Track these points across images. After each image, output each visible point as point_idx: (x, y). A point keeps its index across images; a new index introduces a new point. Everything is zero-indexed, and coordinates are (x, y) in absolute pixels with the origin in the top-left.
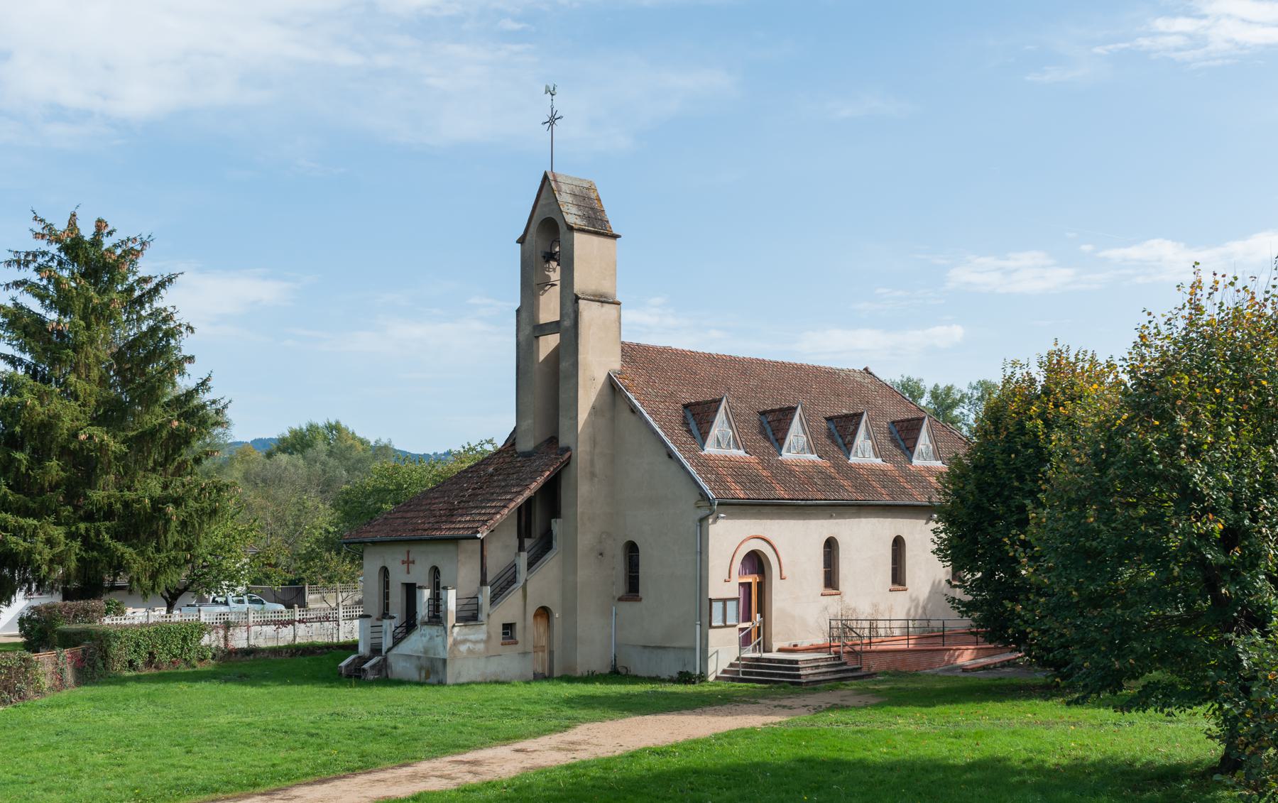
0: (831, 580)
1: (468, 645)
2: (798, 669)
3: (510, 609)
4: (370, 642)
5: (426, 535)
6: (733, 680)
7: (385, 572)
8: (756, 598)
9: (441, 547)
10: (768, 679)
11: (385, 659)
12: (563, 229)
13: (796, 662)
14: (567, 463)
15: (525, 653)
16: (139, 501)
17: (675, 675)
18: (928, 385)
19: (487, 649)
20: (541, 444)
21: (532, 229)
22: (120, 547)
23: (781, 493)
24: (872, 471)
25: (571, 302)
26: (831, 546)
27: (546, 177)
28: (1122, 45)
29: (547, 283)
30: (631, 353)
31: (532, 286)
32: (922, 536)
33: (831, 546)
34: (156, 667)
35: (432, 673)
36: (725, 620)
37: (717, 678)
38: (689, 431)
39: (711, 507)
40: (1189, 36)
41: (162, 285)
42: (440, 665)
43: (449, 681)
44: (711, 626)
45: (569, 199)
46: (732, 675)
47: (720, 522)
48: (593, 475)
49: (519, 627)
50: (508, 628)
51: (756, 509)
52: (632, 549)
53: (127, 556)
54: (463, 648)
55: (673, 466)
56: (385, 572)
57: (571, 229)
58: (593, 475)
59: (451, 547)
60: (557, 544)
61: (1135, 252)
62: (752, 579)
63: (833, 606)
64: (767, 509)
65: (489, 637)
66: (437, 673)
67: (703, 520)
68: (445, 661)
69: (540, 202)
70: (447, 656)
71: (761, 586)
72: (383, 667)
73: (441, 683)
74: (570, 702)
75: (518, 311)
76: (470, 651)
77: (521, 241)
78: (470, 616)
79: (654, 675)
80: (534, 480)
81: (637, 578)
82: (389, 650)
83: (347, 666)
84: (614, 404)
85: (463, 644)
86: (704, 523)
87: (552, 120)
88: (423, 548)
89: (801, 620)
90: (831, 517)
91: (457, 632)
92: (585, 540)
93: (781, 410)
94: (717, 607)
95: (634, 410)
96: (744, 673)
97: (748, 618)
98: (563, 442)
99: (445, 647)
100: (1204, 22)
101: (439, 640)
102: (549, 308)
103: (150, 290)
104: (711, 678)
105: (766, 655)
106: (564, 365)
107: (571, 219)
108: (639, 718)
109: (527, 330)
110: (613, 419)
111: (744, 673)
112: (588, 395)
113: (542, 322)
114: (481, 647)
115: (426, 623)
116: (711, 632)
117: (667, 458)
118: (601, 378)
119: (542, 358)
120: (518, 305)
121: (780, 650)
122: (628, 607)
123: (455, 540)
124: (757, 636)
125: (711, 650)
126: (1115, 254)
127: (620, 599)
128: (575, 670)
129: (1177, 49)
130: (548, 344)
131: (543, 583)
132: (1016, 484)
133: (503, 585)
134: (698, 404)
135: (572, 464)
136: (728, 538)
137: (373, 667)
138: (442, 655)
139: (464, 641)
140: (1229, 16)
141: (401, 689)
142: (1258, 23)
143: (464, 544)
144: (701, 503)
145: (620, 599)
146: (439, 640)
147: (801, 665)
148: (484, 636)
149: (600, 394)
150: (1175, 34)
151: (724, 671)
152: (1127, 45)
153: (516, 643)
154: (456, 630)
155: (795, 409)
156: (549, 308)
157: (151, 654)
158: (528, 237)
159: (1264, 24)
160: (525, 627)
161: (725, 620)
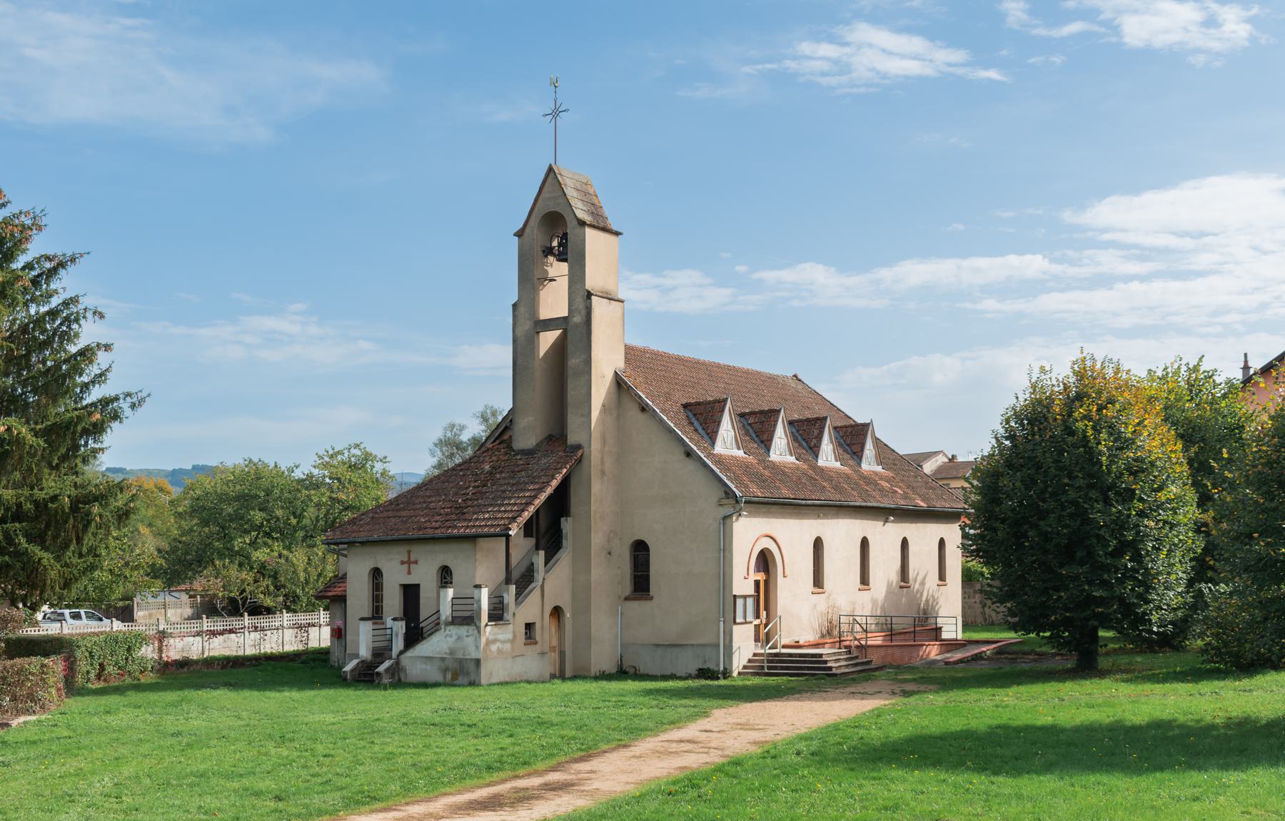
0: (818, 581)
1: (498, 644)
2: (826, 662)
3: (531, 609)
4: (371, 646)
5: (439, 533)
6: (757, 674)
7: (376, 573)
8: (764, 596)
9: (454, 547)
10: (794, 673)
11: (398, 662)
12: (571, 224)
13: (821, 655)
14: (580, 461)
15: (543, 654)
16: (54, 498)
17: (694, 672)
19: (513, 649)
20: (541, 442)
22: (37, 551)
23: (785, 492)
24: (837, 472)
25: (582, 298)
26: (818, 544)
27: (550, 169)
28: (769, 66)
29: (547, 279)
30: (632, 354)
31: (530, 280)
32: (952, 533)
33: (818, 544)
34: (105, 680)
35: (461, 672)
36: (745, 617)
37: (739, 673)
38: (696, 430)
39: (732, 503)
40: (835, 62)
41: (62, 265)
42: (472, 667)
43: (483, 682)
44: (735, 623)
45: (575, 194)
46: (747, 671)
47: (742, 520)
48: (603, 473)
49: (538, 626)
50: (529, 627)
51: (765, 508)
52: (640, 550)
53: (45, 562)
54: (494, 648)
55: (690, 465)
56: (376, 573)
57: (582, 224)
58: (603, 473)
59: (467, 546)
60: (567, 543)
61: (787, 275)
62: (761, 577)
63: (821, 601)
64: (774, 508)
65: (515, 637)
66: (468, 674)
67: (726, 518)
68: (478, 662)
69: (543, 195)
70: (480, 656)
71: (767, 582)
72: (396, 670)
73: (473, 684)
74: (649, 692)
75: (515, 306)
76: (499, 651)
77: (519, 234)
78: (497, 615)
79: (668, 673)
80: (553, 477)
81: (647, 578)
82: (401, 653)
83: (352, 671)
84: (619, 402)
85: (494, 642)
86: (728, 521)
87: (556, 113)
88: (429, 547)
89: (800, 619)
90: (819, 517)
91: (489, 631)
92: (597, 539)
93: (762, 412)
94: (740, 602)
95: (644, 408)
97: (758, 616)
98: (572, 439)
99: (477, 647)
100: (847, 50)
101: (470, 641)
102: (554, 302)
103: (49, 270)
104: (735, 674)
106: (573, 362)
107: (581, 214)
108: (748, 705)
109: (526, 326)
110: (618, 417)
111: (769, 668)
112: (600, 390)
113: (542, 318)
114: (508, 646)
115: (448, 624)
116: (735, 628)
117: (683, 457)
118: (610, 376)
119: (542, 354)
120: (516, 299)
121: (784, 647)
122: (637, 607)
123: (472, 538)
124: (763, 636)
125: (735, 646)
126: (770, 276)
127: (627, 599)
128: (589, 670)
129: (823, 74)
130: (547, 340)
131: (555, 581)
132: (1066, 481)
133: (524, 580)
134: (699, 404)
135: (585, 462)
136: (749, 533)
137: (387, 670)
138: (474, 655)
139: (495, 641)
140: (871, 46)
141: (428, 691)
142: (897, 54)
143: (483, 543)
144: (726, 501)
145: (627, 599)
146: (470, 641)
147: (824, 658)
148: (510, 636)
149: (608, 393)
150: (820, 58)
151: (745, 667)
152: (774, 66)
153: (536, 643)
154: (488, 628)
155: (779, 411)
156: (554, 302)
157: (100, 665)
158: (528, 231)
159: (903, 56)
160: (542, 627)
161: (745, 617)
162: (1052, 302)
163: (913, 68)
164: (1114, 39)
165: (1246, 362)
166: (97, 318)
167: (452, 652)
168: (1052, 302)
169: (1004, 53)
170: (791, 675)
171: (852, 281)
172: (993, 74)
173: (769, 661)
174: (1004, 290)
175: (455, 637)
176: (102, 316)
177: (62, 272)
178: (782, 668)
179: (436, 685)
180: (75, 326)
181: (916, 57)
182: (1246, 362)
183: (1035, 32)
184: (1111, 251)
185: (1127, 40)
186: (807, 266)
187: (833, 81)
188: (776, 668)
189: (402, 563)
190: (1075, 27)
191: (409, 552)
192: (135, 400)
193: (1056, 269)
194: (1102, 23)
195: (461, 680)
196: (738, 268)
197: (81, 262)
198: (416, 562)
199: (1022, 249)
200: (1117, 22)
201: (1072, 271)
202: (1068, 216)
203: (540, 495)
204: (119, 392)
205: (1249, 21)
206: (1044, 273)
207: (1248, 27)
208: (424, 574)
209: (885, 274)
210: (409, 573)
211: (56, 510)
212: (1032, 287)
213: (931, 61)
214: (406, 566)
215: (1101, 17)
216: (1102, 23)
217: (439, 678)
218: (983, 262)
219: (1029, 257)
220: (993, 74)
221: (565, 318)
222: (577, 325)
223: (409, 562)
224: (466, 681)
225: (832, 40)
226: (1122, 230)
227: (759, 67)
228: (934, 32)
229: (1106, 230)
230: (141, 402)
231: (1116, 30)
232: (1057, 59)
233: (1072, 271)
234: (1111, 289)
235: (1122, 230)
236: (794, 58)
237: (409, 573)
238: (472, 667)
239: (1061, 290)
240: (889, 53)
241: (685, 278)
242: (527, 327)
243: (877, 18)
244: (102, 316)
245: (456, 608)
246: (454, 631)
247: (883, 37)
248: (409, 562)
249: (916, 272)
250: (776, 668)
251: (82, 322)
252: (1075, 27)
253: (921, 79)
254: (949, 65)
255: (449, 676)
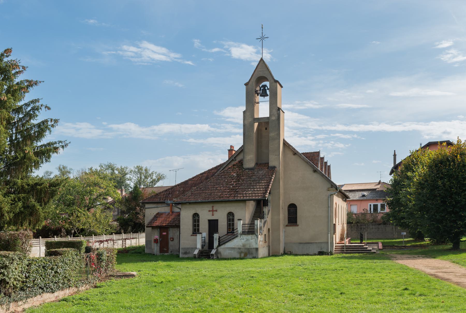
7: (196, 217)
17: (317, 253)
18: (132, 167)
21: (252, 80)
25: (276, 111)
40: (136, 53)
42: (254, 251)
43: (260, 256)
56: (196, 217)
59: (241, 204)
61: (121, 126)
66: (252, 254)
77: (246, 84)
86: (332, 196)
88: (223, 205)
96: (346, 251)
100: (140, 50)
101: (253, 241)
105: (382, 241)
109: (251, 120)
111: (346, 251)
115: (241, 234)
117: (312, 172)
120: (244, 108)
123: (244, 201)
126: (115, 126)
129: (132, 57)
138: (255, 246)
140: (148, 49)
145: (287, 226)
150: (130, 52)
152: (114, 53)
158: (250, 83)
162: (212, 140)
163: (163, 58)
164: (229, 55)
165: (395, 153)
166: (47, 109)
167: (244, 245)
168: (212, 140)
169: (193, 56)
170: (362, 253)
171: (144, 130)
172: (190, 63)
173: (346, 248)
174: (198, 135)
175: (245, 240)
176: (49, 109)
177: (31, 89)
178: (350, 251)
179: (234, 259)
180: (36, 112)
181: (163, 54)
182: (395, 153)
183: (203, 50)
184: (230, 124)
185: (233, 55)
186: (128, 123)
187: (136, 60)
188: (348, 251)
189: (209, 211)
190: (216, 50)
191: (213, 207)
192: (63, 144)
193: (212, 129)
194: (225, 49)
195: (248, 256)
196: (104, 123)
197: (40, 85)
198: (216, 211)
199: (202, 122)
200: (230, 49)
201: (218, 130)
202: (215, 112)
203: (253, 185)
204: (57, 141)
205: (270, 53)
206: (209, 131)
207: (270, 55)
208: (221, 215)
209: (156, 128)
210: (213, 215)
211: (41, 189)
212: (205, 135)
213: (169, 56)
214: (212, 212)
215: (225, 47)
216: (225, 49)
217: (238, 256)
218: (189, 126)
219: (204, 125)
220: (190, 63)
221: (268, 118)
222: (273, 121)
223: (213, 211)
224: (251, 257)
225: (135, 45)
226: (233, 118)
227: (109, 52)
228: (170, 46)
229: (228, 118)
230: (66, 145)
231: (230, 52)
232: (211, 60)
233: (218, 130)
234: (230, 137)
235: (233, 118)
236: (121, 50)
237: (213, 215)
238: (254, 251)
239: (215, 137)
240: (154, 52)
241: (84, 125)
242: (250, 121)
243: (150, 40)
244: (49, 109)
245: (244, 228)
246: (245, 237)
247: (152, 47)
248: (213, 211)
249: (166, 128)
250: (348, 251)
251: (40, 110)
252: (216, 50)
253: (165, 62)
254: (175, 58)
255: (243, 255)
